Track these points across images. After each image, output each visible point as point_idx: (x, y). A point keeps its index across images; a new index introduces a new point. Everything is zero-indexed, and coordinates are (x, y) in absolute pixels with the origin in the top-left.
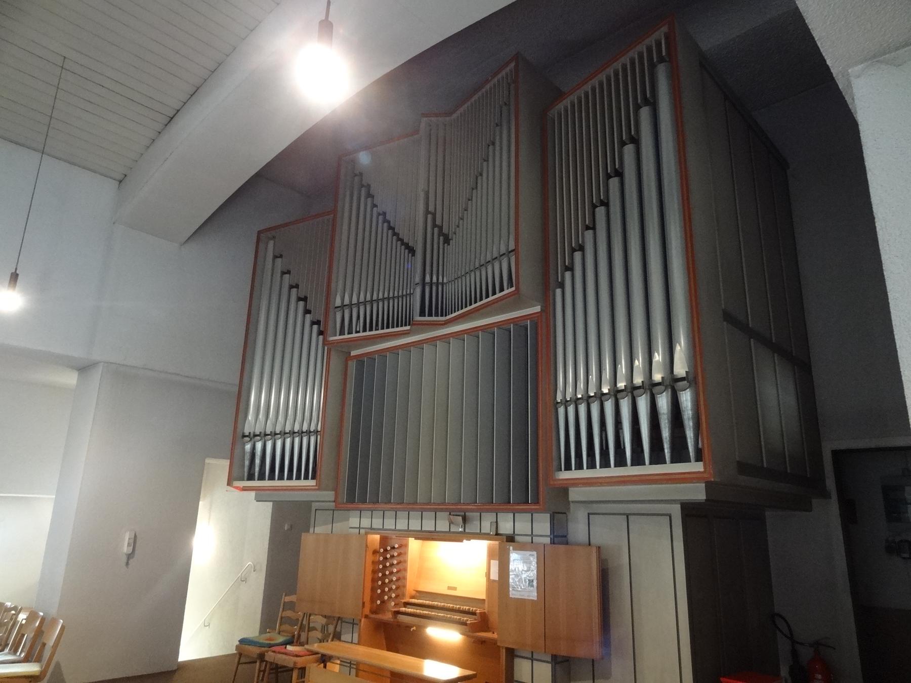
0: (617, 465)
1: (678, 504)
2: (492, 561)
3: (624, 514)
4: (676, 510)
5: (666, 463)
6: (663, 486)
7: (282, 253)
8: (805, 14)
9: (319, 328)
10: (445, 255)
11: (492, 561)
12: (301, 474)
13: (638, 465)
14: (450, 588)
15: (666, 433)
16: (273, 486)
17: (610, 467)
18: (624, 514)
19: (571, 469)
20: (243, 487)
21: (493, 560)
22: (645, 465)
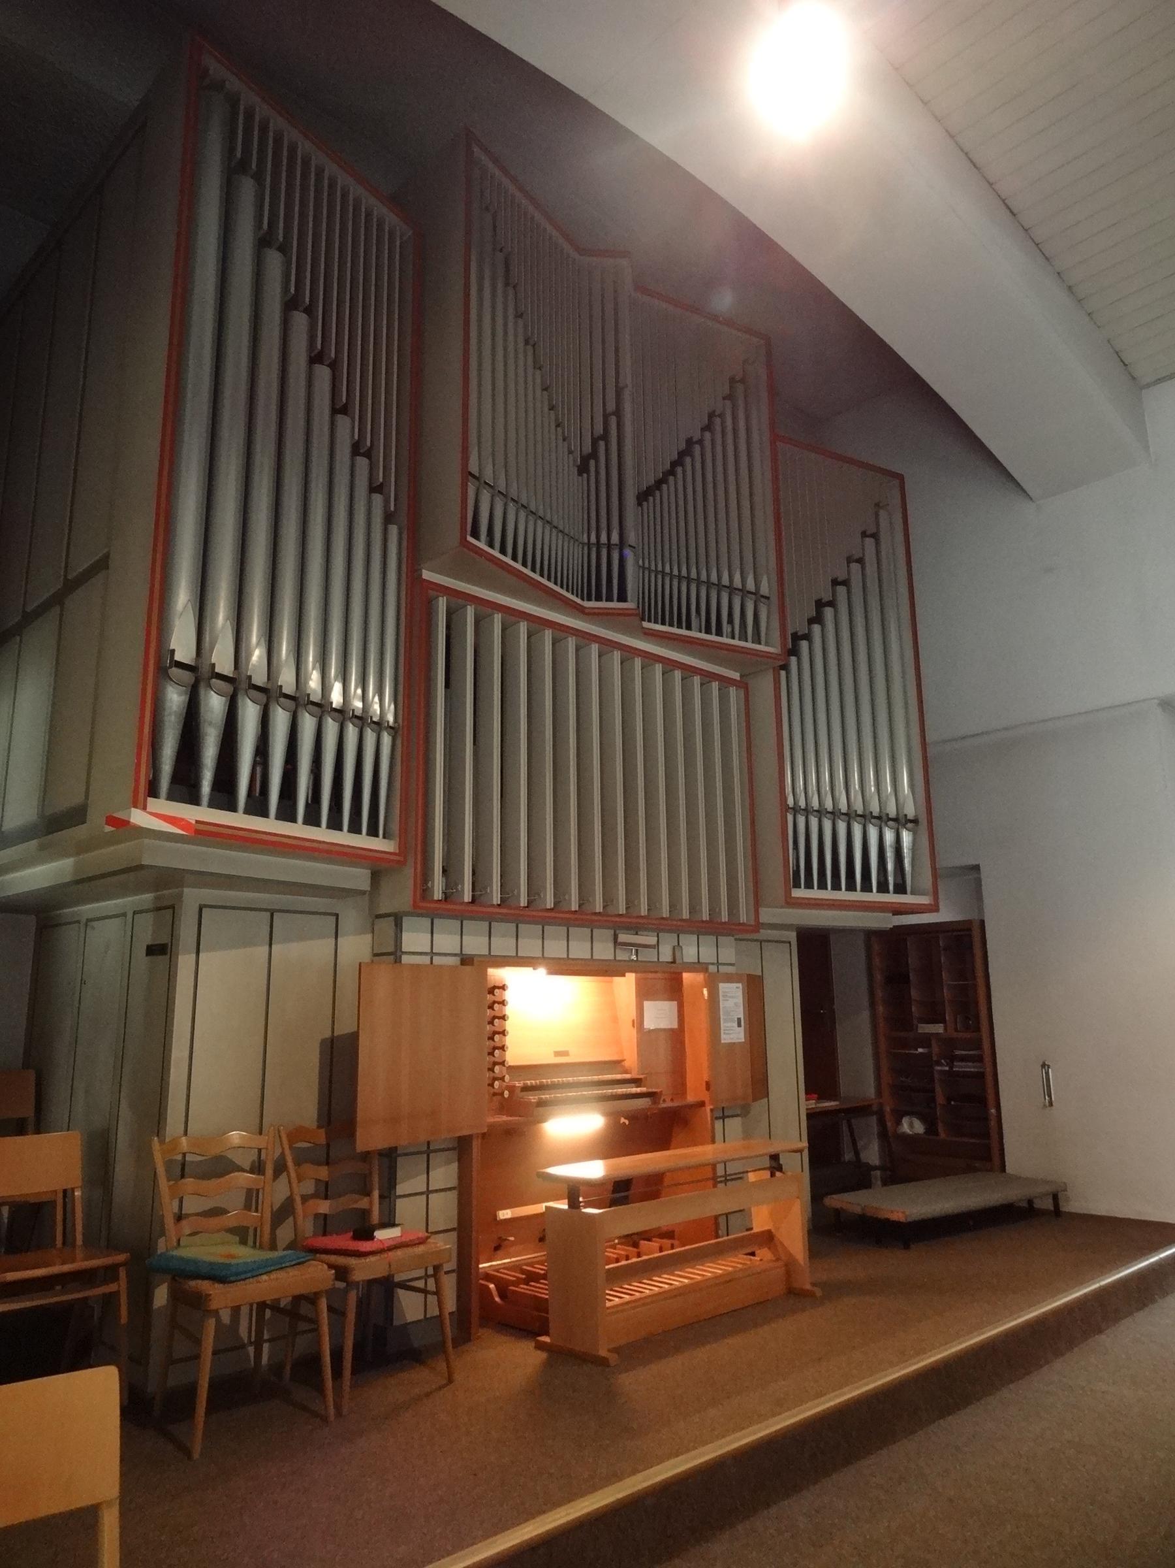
0: (820, 887)
1: (792, 931)
2: (647, 1004)
3: (266, 910)
4: (792, 936)
5: (856, 891)
6: (851, 913)
7: (815, 598)
8: (528, 188)
9: (386, 502)
10: (585, 495)
11: (647, 1004)
12: (812, 879)
13: (851, 891)
14: (558, 1054)
15: (890, 866)
16: (275, 835)
17: (855, 890)
18: (266, 910)
19: (840, 889)
20: (197, 822)
21: (647, 1000)
22: (856, 891)
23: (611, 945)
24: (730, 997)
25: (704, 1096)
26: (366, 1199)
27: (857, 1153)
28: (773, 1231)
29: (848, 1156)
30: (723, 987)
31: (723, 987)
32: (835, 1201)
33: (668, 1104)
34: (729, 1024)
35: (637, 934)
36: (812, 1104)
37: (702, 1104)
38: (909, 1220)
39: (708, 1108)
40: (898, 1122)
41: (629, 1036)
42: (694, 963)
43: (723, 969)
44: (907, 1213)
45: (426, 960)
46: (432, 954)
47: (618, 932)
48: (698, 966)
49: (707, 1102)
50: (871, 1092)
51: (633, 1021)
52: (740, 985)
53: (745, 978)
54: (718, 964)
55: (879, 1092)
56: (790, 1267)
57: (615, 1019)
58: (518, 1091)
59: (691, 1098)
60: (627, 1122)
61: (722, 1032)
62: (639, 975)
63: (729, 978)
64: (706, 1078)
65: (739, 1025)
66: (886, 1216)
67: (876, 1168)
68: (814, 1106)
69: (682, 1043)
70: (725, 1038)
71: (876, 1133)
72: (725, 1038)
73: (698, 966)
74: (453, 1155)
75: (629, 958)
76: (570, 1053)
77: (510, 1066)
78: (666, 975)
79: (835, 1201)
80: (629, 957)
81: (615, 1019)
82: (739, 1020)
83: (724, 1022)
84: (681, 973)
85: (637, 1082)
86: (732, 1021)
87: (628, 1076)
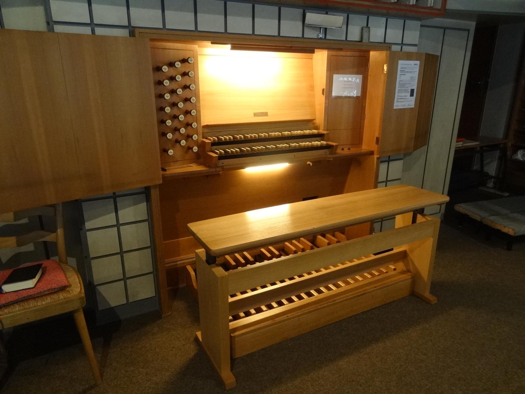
2: (336, 77)
21: (337, 73)
23: (300, 24)
24: (408, 72)
25: (374, 147)
26: (54, 235)
27: (482, 166)
28: (407, 251)
29: (476, 167)
30: (402, 63)
31: (402, 63)
32: (462, 208)
33: (346, 152)
34: (403, 94)
35: (327, 13)
36: (460, 144)
37: (372, 153)
38: (518, 234)
39: (376, 156)
40: (515, 152)
41: (320, 101)
42: (381, 43)
43: (406, 49)
44: (516, 231)
45: (87, 30)
46: (92, 24)
47: (306, 11)
48: (384, 46)
49: (375, 153)
50: (500, 134)
51: (323, 90)
52: (418, 62)
53: (424, 58)
54: (402, 44)
55: (506, 135)
56: (416, 278)
57: (312, 88)
58: (208, 147)
59: (365, 148)
60: (311, 164)
61: (396, 100)
62: (334, 53)
63: (409, 56)
64: (377, 135)
65: (412, 95)
66: (499, 228)
67: (492, 177)
68: (461, 146)
69: (363, 108)
70: (398, 105)
71: (497, 157)
72: (398, 105)
73: (384, 46)
74: (143, 196)
75: (318, 35)
76: (269, 114)
77: (207, 126)
78: (357, 54)
79: (462, 208)
80: (318, 35)
81: (312, 88)
82: (412, 91)
83: (398, 93)
84: (368, 52)
85: (320, 136)
86: (406, 91)
87: (315, 131)
